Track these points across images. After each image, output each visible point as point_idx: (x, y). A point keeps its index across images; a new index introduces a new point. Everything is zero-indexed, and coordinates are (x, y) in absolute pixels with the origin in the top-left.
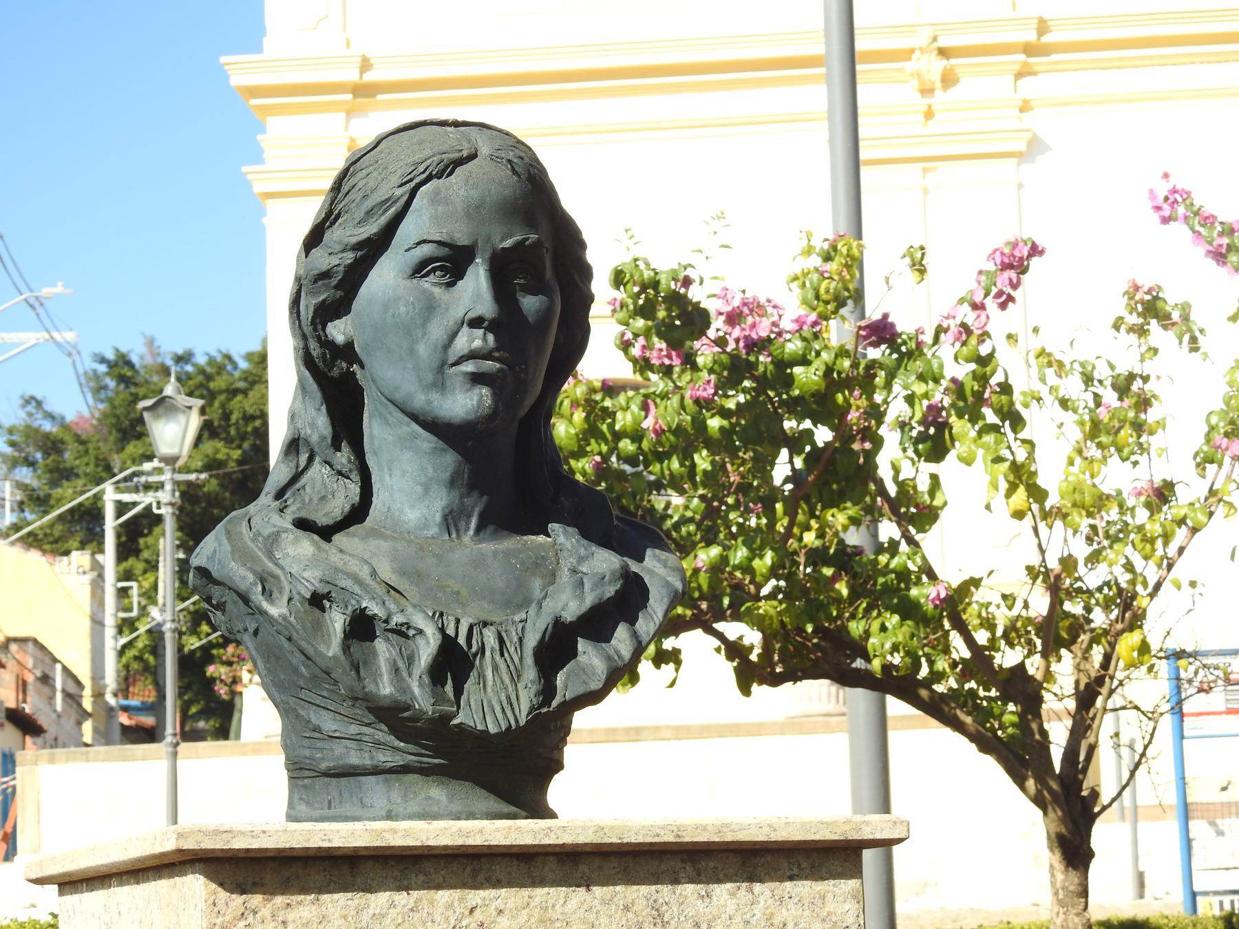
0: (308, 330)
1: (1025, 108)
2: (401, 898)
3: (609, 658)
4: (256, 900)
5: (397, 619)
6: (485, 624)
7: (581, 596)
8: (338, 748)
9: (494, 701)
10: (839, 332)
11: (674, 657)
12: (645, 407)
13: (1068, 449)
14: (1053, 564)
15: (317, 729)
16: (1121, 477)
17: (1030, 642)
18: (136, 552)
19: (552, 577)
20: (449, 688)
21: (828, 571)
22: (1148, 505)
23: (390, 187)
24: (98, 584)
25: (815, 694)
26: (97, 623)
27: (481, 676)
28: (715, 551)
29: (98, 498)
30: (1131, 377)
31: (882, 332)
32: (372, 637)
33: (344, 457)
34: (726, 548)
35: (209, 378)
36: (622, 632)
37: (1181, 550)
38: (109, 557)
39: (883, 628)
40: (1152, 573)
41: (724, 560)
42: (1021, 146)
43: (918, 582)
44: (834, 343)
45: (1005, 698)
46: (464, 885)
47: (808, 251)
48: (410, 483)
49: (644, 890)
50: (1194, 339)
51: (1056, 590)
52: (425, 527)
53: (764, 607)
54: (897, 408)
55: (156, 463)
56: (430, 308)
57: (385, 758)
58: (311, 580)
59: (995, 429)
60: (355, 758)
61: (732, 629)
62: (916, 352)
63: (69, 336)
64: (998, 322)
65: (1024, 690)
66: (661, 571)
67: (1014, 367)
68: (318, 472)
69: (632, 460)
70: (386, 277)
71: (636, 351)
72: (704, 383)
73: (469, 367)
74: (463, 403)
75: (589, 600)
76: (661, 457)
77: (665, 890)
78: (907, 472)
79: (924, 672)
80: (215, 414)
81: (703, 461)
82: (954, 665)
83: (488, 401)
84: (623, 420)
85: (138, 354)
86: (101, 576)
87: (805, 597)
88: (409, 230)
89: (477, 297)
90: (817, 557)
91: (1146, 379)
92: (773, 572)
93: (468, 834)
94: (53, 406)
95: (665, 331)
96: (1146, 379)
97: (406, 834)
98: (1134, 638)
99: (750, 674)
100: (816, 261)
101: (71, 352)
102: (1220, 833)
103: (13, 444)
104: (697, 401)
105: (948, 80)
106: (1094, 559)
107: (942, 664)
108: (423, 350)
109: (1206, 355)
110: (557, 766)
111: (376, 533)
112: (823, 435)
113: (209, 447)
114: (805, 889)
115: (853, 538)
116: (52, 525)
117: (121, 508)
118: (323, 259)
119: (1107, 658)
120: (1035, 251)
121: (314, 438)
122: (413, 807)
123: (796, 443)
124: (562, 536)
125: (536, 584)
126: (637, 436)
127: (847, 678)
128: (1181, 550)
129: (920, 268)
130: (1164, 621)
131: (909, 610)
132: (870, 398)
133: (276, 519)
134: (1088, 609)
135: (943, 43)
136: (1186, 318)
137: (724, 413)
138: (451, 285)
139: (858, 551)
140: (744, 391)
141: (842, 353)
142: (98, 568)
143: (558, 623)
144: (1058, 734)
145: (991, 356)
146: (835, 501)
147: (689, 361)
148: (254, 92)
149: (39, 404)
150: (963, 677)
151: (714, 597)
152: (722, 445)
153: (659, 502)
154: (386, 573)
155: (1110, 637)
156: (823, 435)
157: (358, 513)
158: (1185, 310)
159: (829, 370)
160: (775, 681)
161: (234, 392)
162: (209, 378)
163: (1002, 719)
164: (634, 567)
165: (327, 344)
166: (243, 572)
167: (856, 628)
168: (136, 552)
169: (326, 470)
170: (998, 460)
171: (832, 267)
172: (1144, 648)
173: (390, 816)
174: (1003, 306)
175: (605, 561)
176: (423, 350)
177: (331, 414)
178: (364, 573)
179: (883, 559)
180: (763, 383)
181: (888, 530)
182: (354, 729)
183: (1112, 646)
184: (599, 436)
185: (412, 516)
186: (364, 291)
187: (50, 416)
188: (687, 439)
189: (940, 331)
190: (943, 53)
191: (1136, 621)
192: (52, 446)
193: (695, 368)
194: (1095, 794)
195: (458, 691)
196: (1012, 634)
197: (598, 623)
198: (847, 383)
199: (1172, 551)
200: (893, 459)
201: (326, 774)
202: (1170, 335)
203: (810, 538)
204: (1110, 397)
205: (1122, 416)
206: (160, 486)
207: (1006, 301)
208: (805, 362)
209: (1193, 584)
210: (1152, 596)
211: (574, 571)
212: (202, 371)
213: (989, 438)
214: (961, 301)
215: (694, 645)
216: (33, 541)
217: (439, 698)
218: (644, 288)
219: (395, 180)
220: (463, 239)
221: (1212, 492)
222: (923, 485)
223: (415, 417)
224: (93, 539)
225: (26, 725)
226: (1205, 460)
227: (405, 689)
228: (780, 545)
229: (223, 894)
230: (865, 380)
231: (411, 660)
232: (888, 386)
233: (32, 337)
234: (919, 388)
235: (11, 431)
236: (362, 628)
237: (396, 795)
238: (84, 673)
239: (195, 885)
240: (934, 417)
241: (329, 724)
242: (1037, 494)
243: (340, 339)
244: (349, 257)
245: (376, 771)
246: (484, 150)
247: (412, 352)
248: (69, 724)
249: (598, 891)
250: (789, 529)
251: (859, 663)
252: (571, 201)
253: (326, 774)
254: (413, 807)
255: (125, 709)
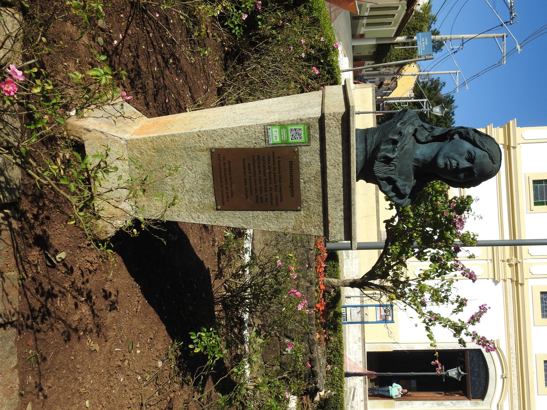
0: (457, 130)
1: (505, 280)
2: (341, 151)
3: (388, 191)
4: (340, 122)
5: (396, 149)
6: (395, 167)
7: (401, 186)
8: (370, 138)
9: (379, 168)
10: (457, 240)
11: (391, 208)
12: (442, 202)
13: (433, 285)
14: (410, 282)
15: (375, 134)
16: (427, 295)
17: (394, 277)
18: (414, 106)
19: (405, 180)
20: (382, 160)
21: (408, 238)
22: (421, 301)
23: (487, 146)
24: (407, 98)
25: (384, 236)
26: (400, 98)
27: (385, 166)
28: (412, 216)
29: (425, 98)
30: (448, 299)
31: (457, 250)
32: (393, 144)
33: (430, 138)
34: (413, 218)
35: (449, 119)
36: (394, 194)
37: (412, 307)
38: (413, 100)
39: (397, 249)
40: (407, 301)
41: (411, 217)
42: (496, 279)
43: (406, 256)
44: (455, 240)
45: (383, 272)
46: (343, 163)
47: (474, 235)
48: (424, 151)
49: (342, 198)
50: (455, 312)
51: (405, 282)
52: (415, 155)
53: (401, 225)
54: (441, 252)
55: (431, 107)
56: (461, 155)
57: (369, 147)
58: (405, 132)
59: (437, 272)
60: (368, 141)
61: (397, 219)
62: (452, 256)
63: (458, 91)
64: (459, 273)
65: (384, 276)
66: (406, 202)
67: (449, 275)
68: (427, 133)
69: (431, 199)
70: (468, 146)
71: (453, 200)
72: (447, 214)
73: (448, 163)
74: (441, 162)
75: (400, 188)
76: (432, 206)
77: (342, 202)
78: (428, 254)
79: (388, 257)
80: (442, 120)
81: (430, 213)
82: (390, 262)
83: (441, 167)
84: (440, 198)
85: (455, 104)
86: (409, 99)
87: (403, 233)
88: (478, 151)
89: (463, 164)
90: (411, 236)
91: (447, 302)
92: (408, 227)
93: (353, 164)
94: (443, 88)
95: (458, 206)
96: (447, 302)
97: (353, 151)
98: (395, 297)
99: (388, 223)
100: (472, 237)
101: (454, 91)
102: (358, 313)
103: (436, 81)
104: (443, 212)
105: (510, 265)
106: (410, 290)
107: (390, 260)
108: (452, 154)
109: (452, 314)
110: (367, 182)
111: (414, 145)
112: (436, 237)
113: (435, 119)
114: (342, 229)
115: (415, 243)
116: (419, 89)
117: (423, 102)
118: (472, 133)
119: (391, 292)
120: (474, 281)
121: (434, 132)
122: (359, 153)
123: (434, 232)
124: (413, 182)
125: (404, 177)
126: (436, 200)
127: (387, 241)
128: (412, 307)
129: (470, 257)
130: (399, 304)
131: (400, 254)
132: (443, 247)
133: (417, 125)
134: (400, 289)
135: (519, 264)
136: (460, 311)
137: (441, 218)
138: (466, 159)
139: (412, 244)
140: (445, 222)
141: (453, 241)
142: (411, 98)
143: (396, 181)
144: (377, 282)
145: (452, 271)
146: (422, 240)
147: (451, 211)
148: (509, 125)
149: (444, 86)
150: (387, 264)
151: (403, 216)
152: (434, 217)
153: (422, 205)
154: (406, 147)
155: (395, 293)
156: (436, 237)
157: (418, 141)
158: (462, 311)
159: (449, 239)
160: (386, 227)
161: (446, 124)
162: (449, 119)
163: (379, 271)
164: (407, 197)
165: (454, 134)
166: (406, 118)
167: (397, 243)
168: (414, 106)
169: (427, 135)
170: (430, 272)
171: (471, 240)
172: (393, 299)
173: (357, 149)
174: (462, 274)
175: (408, 191)
176: (452, 154)
177: (439, 135)
178: (406, 143)
179: (411, 249)
180: (447, 226)
181: (417, 250)
182: (374, 141)
183: (393, 293)
184: (436, 193)
185: (418, 152)
186: (465, 141)
187: (441, 88)
188: (435, 210)
189: (457, 261)
190: (516, 264)
191: (398, 298)
192: (435, 88)
193: (450, 212)
194: (364, 289)
195: (382, 162)
196: (396, 274)
197: (395, 189)
198: (446, 242)
199: (412, 305)
200: (431, 251)
201: (366, 136)
202: (456, 307)
203: (415, 234)
204: (443, 295)
205: (439, 297)
206: (427, 108)
207: (463, 274)
208: (451, 234)
209: (405, 309)
210: (403, 301)
211: (406, 185)
212: (450, 117)
213: (435, 270)
214: (463, 265)
215: (394, 212)
216: (416, 85)
217: (381, 158)
218: (467, 202)
219: (489, 147)
220: (475, 161)
221: (424, 314)
222: (426, 257)
223: (438, 152)
224: (416, 97)
225: (380, 85)
226: (430, 312)
227: (382, 151)
228: (414, 229)
229: (341, 115)
230: (447, 246)
231: (388, 152)
232: (446, 250)
233: (457, 83)
234: (445, 257)
235: (438, 80)
236: (395, 142)
237: (361, 150)
238: (390, 96)
239: (343, 110)
240: (439, 260)
241: (375, 136)
242: (424, 280)
243: (455, 137)
244: (472, 138)
245: (366, 146)
246: (495, 166)
247: (452, 151)
248: (380, 94)
249: (342, 189)
250: (417, 230)
251: (390, 244)
252: (484, 184)
253: (366, 136)
254: (359, 153)
255: (383, 105)
